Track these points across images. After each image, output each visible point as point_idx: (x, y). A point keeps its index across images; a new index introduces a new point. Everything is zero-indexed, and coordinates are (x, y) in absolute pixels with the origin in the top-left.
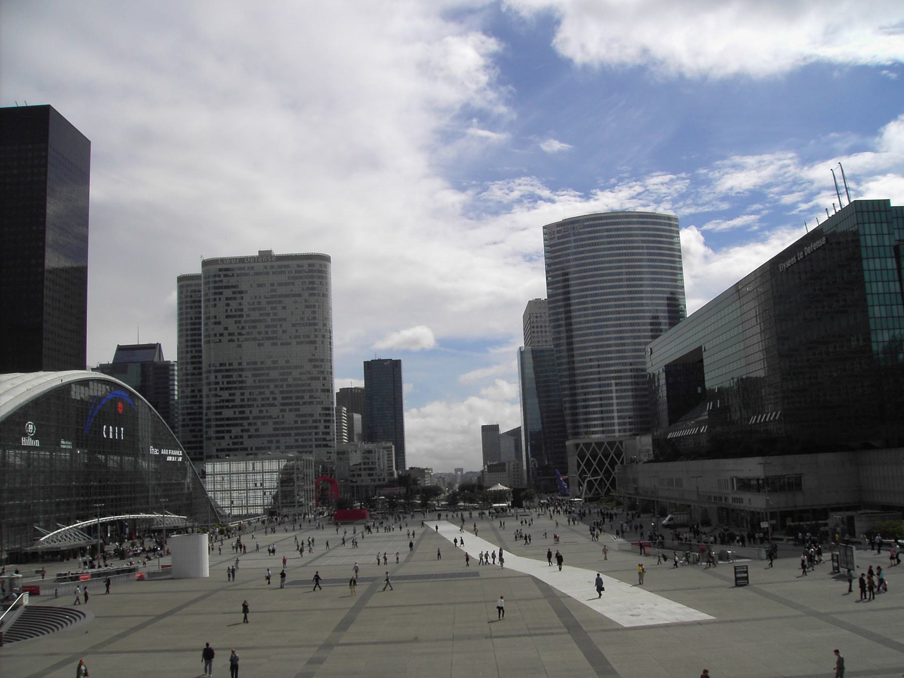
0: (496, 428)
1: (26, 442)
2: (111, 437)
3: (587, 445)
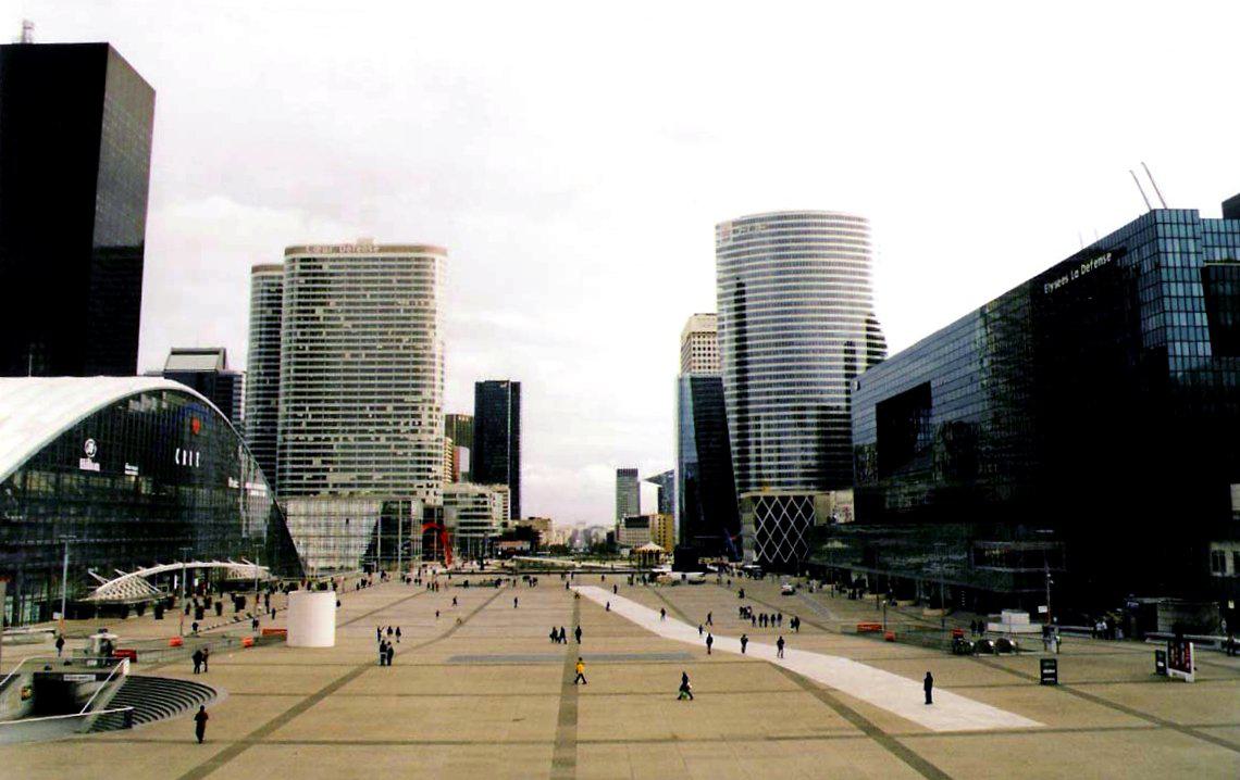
0: (633, 473)
1: (86, 464)
2: (184, 463)
3: (769, 499)
